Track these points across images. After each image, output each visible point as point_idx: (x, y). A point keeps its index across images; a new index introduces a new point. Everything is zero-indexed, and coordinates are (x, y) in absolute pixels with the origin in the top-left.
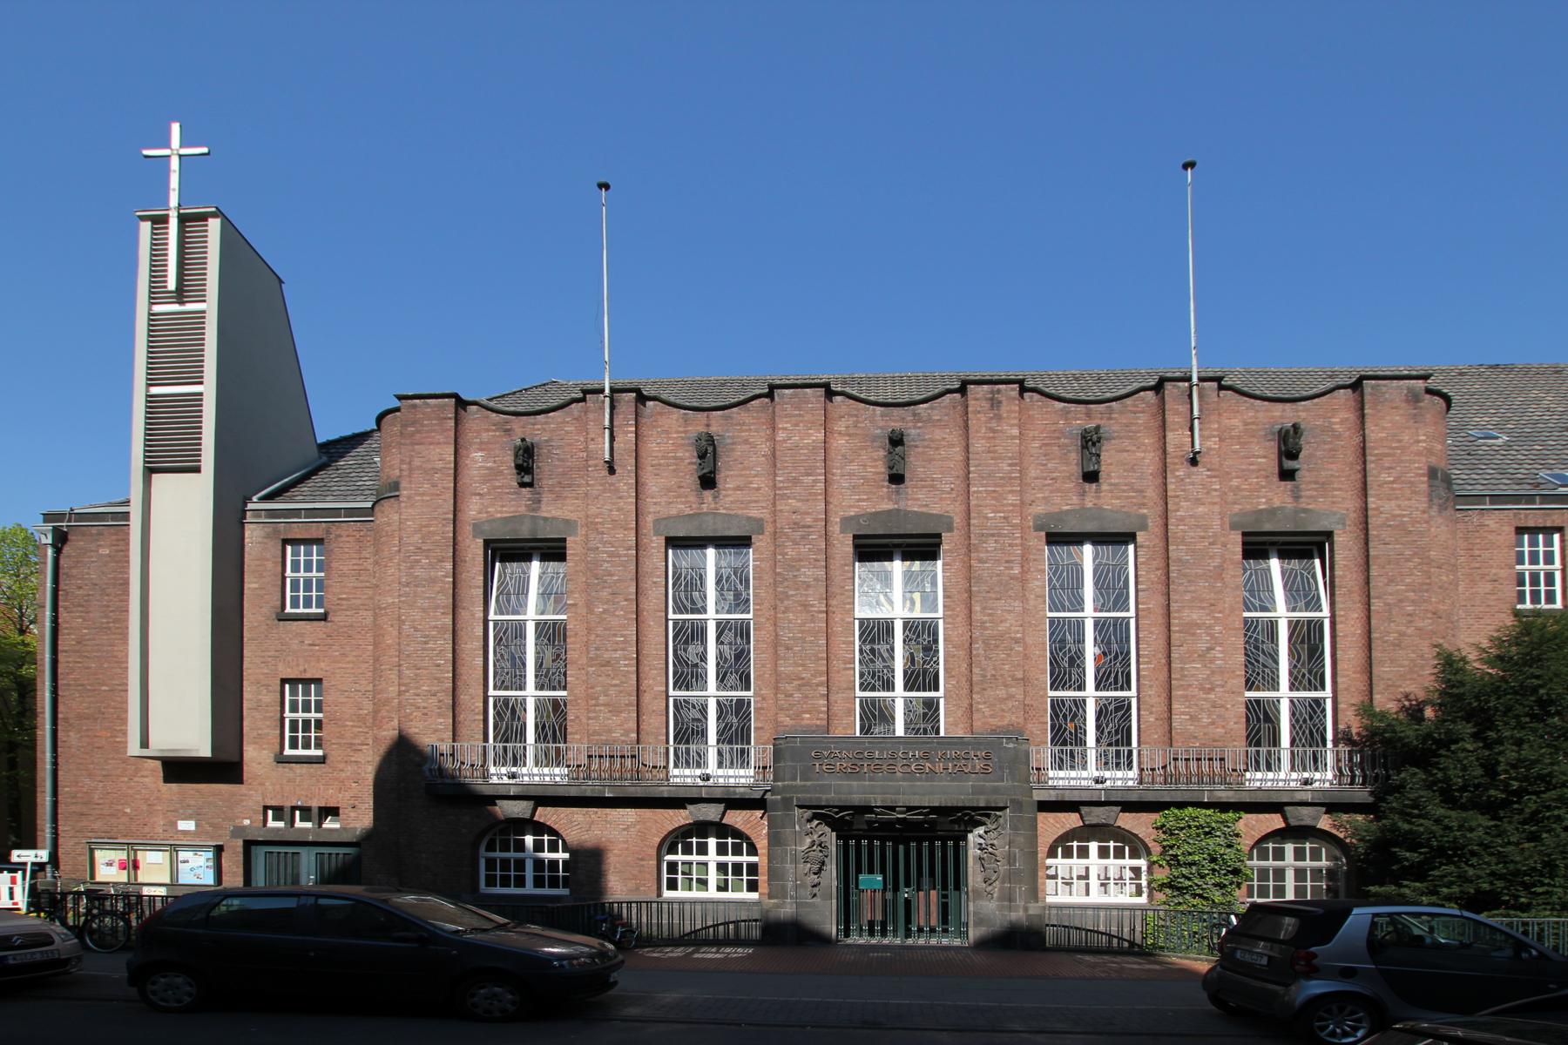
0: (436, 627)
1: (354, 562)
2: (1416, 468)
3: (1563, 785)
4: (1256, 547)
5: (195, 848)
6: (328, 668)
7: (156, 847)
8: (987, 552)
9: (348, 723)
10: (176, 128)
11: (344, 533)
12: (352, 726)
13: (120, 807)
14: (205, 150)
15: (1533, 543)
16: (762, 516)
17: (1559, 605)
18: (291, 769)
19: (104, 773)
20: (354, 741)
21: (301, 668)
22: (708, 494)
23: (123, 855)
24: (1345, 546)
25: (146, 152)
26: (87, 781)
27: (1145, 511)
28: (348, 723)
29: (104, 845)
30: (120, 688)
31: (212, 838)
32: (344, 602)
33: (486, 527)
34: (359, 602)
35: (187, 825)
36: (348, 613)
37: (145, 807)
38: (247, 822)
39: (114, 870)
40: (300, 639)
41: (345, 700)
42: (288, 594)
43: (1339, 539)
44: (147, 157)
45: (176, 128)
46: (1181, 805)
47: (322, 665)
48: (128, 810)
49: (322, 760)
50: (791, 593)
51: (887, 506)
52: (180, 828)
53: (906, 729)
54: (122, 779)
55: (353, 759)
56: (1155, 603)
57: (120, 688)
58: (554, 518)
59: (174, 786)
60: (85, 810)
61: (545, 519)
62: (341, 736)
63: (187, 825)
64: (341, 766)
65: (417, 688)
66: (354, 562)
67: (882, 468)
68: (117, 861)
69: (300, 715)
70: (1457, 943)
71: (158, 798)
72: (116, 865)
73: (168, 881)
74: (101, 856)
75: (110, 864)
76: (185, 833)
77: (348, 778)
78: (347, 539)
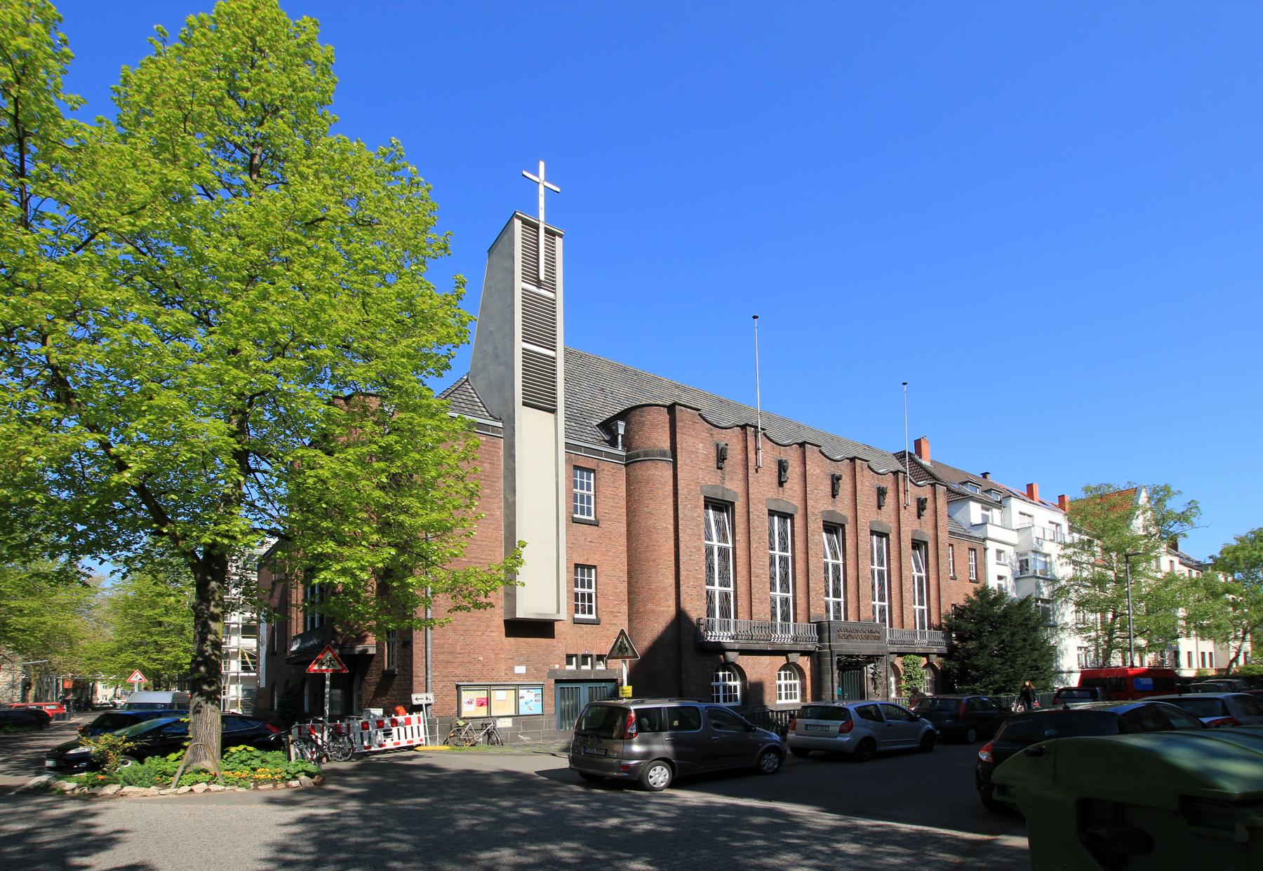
0: (694, 547)
1: (612, 489)
4: (772, 513)
5: (529, 686)
7: (503, 686)
10: (542, 165)
11: (606, 469)
13: (476, 656)
14: (558, 190)
15: (582, 477)
18: (581, 628)
19: (464, 628)
20: (614, 610)
22: (781, 489)
23: (483, 694)
24: (848, 528)
25: (525, 173)
26: (452, 634)
29: (470, 687)
30: (475, 560)
31: (536, 678)
33: (705, 489)
34: (614, 516)
35: (520, 669)
37: (493, 656)
38: (557, 666)
39: (473, 707)
42: (593, 506)
45: (542, 165)
46: (910, 654)
47: (597, 556)
48: (481, 659)
49: (596, 622)
54: (477, 633)
57: (475, 560)
59: (512, 639)
60: (450, 658)
62: (607, 607)
63: (520, 669)
64: (608, 626)
66: (612, 489)
67: (715, 466)
68: (475, 700)
69: (586, 590)
70: (210, 541)
71: (501, 649)
72: (474, 702)
73: (513, 713)
74: (466, 696)
75: (470, 703)
76: (519, 675)
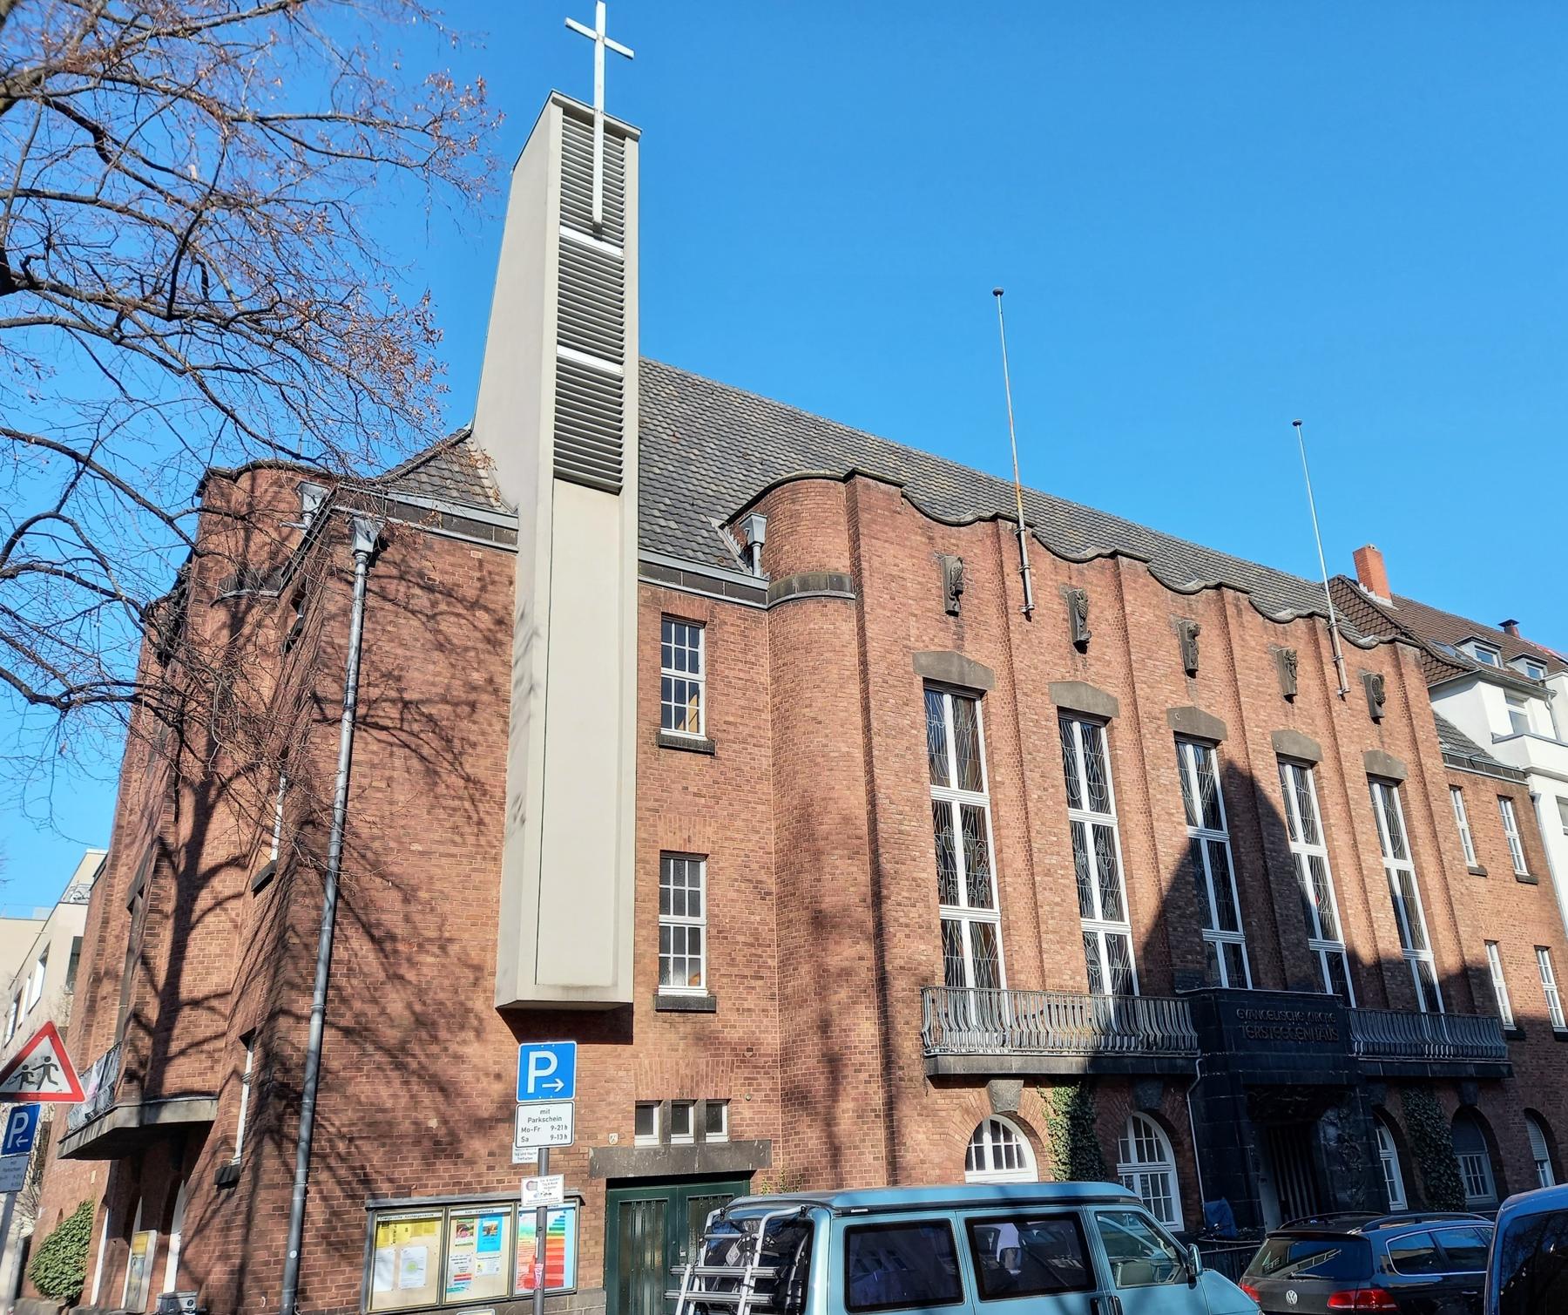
10: (601, 9)
12: (745, 944)
16: (1115, 695)
32: (732, 729)
47: (709, 831)
50: (1159, 797)
58: (976, 663)
61: (969, 662)
78: (732, 629)
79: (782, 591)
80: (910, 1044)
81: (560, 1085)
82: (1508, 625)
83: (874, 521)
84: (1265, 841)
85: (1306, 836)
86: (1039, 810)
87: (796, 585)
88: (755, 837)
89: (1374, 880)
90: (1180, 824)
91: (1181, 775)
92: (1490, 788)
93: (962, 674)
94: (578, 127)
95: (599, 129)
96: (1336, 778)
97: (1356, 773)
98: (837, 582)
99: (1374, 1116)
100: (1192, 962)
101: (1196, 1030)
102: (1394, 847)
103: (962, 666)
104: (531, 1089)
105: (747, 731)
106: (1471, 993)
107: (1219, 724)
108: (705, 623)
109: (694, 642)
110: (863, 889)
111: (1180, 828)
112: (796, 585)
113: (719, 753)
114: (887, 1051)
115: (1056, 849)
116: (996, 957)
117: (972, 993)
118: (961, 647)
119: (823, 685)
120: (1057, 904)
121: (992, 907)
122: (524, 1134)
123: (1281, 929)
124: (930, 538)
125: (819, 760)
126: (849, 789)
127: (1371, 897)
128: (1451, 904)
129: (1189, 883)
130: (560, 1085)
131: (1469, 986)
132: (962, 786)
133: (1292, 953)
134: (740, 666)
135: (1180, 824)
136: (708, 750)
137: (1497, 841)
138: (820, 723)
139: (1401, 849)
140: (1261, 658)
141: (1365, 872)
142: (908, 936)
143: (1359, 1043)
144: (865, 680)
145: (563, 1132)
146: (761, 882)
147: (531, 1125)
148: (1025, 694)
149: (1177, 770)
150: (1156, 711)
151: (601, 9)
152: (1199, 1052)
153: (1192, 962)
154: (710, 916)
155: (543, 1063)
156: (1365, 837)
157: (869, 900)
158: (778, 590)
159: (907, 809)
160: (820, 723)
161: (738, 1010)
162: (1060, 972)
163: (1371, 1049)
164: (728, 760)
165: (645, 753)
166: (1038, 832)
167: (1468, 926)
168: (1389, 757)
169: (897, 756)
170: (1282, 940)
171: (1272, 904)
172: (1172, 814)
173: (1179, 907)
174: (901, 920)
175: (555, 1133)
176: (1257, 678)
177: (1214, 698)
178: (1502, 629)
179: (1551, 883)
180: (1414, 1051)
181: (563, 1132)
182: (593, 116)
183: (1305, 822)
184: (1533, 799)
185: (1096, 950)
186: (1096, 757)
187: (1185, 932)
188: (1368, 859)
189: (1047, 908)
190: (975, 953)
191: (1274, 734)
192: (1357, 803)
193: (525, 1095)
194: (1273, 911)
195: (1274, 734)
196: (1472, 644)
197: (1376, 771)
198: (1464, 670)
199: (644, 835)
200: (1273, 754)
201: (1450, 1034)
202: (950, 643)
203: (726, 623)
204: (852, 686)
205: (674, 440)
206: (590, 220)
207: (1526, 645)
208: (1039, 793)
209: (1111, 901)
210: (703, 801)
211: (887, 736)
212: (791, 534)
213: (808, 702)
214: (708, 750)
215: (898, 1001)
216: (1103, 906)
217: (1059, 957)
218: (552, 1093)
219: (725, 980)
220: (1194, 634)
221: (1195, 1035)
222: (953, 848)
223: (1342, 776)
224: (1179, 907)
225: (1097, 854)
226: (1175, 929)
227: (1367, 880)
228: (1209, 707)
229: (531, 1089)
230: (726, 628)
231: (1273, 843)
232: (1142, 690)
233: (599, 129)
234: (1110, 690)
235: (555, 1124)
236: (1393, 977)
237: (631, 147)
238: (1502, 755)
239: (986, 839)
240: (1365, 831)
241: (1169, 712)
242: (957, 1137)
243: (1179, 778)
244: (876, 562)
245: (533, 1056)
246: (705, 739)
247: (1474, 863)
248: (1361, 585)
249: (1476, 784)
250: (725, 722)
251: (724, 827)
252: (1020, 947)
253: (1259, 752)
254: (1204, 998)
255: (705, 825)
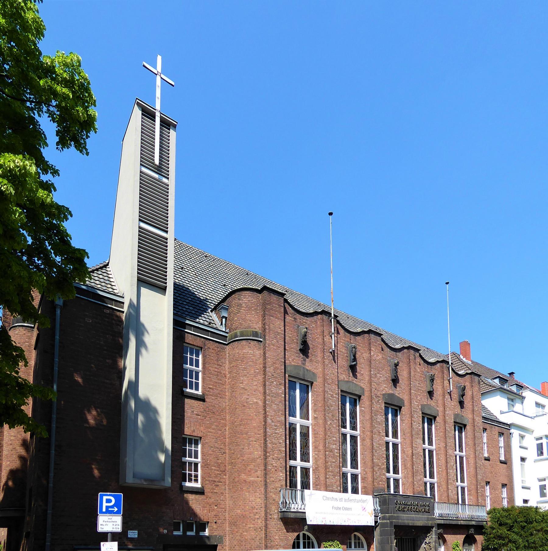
2: (215, 368)
3: (436, 549)
6: (204, 431)
8: (415, 418)
9: (213, 468)
10: (159, 58)
12: (215, 470)
16: (364, 387)
17: (137, 531)
21: (192, 429)
27: (438, 408)
28: (213, 468)
32: (211, 390)
36: (213, 398)
40: (192, 410)
41: (212, 453)
43: (468, 427)
44: (144, 66)
47: (202, 428)
50: (376, 426)
51: (391, 392)
52: (129, 536)
53: (394, 492)
55: (215, 491)
56: (442, 445)
58: (310, 371)
61: (307, 370)
64: (210, 494)
65: (273, 455)
77: (213, 503)
78: (213, 351)
79: (233, 337)
80: (274, 507)
81: (116, 509)
82: (511, 374)
83: (272, 309)
84: (414, 444)
85: (429, 443)
86: (330, 428)
87: (239, 334)
88: (220, 432)
89: (451, 459)
90: (383, 436)
91: (385, 419)
92: (496, 430)
93: (304, 375)
94: (148, 121)
95: (158, 120)
96: (442, 423)
97: (451, 421)
98: (256, 334)
99: (438, 536)
100: (381, 485)
101: (380, 506)
102: (459, 448)
103: (304, 372)
104: (104, 510)
105: (218, 392)
106: (478, 498)
107: (402, 400)
108: (201, 348)
109: (197, 356)
110: (260, 453)
111: (383, 438)
112: (239, 334)
113: (206, 400)
114: (266, 509)
115: (335, 442)
116: (309, 479)
117: (298, 491)
118: (304, 364)
119: (248, 375)
120: (334, 462)
121: (309, 462)
122: (101, 526)
123: (415, 474)
124: (295, 319)
125: (245, 404)
126: (256, 416)
127: (449, 465)
128: (476, 468)
129: (384, 457)
130: (116, 509)
131: (478, 496)
132: (301, 418)
133: (417, 483)
134: (216, 366)
135: (383, 436)
136: (201, 399)
137: (495, 448)
138: (246, 390)
139: (462, 449)
140: (421, 376)
141: (448, 456)
142: (276, 470)
143: (437, 512)
144: (265, 374)
145: (118, 527)
146: (222, 449)
147: (104, 523)
148: (329, 384)
149: (384, 417)
150: (379, 394)
151: (159, 58)
152: (380, 514)
153: (381, 485)
154: (202, 459)
155: (109, 501)
156: (450, 444)
157: (262, 457)
158: (232, 336)
159: (278, 424)
160: (246, 390)
161: (212, 492)
162: (332, 486)
163: (440, 515)
164: (210, 402)
165: (177, 397)
166: (329, 436)
167: (481, 476)
168: (463, 416)
169: (276, 404)
170: (415, 478)
171: (413, 466)
172: (380, 432)
173: (379, 466)
174: (274, 465)
175: (114, 527)
176: (419, 384)
177: (401, 391)
178: (509, 375)
179: (511, 463)
180: (455, 516)
181: (118, 527)
182: (155, 112)
183: (429, 438)
184: (511, 434)
185: (347, 479)
186: (354, 410)
187: (380, 474)
188: (450, 452)
189: (329, 463)
190: (301, 477)
191: (422, 405)
192: (449, 432)
193: (102, 512)
194: (413, 468)
195: (422, 405)
196: (498, 379)
197: (457, 421)
198: (494, 387)
199: (176, 428)
200: (421, 413)
201: (468, 511)
202: (300, 362)
203: (210, 349)
204: (259, 376)
205: (196, 276)
206: (153, 163)
207: (516, 381)
208: (330, 422)
209: (354, 462)
210: (199, 417)
211: (272, 396)
212: (238, 313)
213: (241, 381)
214: (201, 399)
215: (271, 492)
216: (351, 464)
217: (333, 481)
218: (112, 512)
219: (207, 482)
220: (396, 365)
221: (379, 508)
222: (296, 440)
223: (445, 422)
224: (379, 466)
225: (351, 446)
226: (376, 473)
227: (448, 459)
228: (399, 394)
229: (104, 510)
230: (211, 350)
231: (416, 445)
232: (374, 385)
233: (158, 120)
234: (362, 385)
235: (115, 523)
236: (452, 492)
237: (173, 134)
238: (503, 418)
239: (309, 437)
240: (450, 441)
241: (383, 395)
242: (290, 538)
243: (384, 420)
244: (272, 326)
245: (105, 498)
246: (201, 394)
247: (486, 455)
248: (461, 356)
249: (492, 428)
250: (209, 388)
251: (207, 428)
252: (318, 477)
253: (416, 411)
254: (384, 497)
255: (200, 426)
